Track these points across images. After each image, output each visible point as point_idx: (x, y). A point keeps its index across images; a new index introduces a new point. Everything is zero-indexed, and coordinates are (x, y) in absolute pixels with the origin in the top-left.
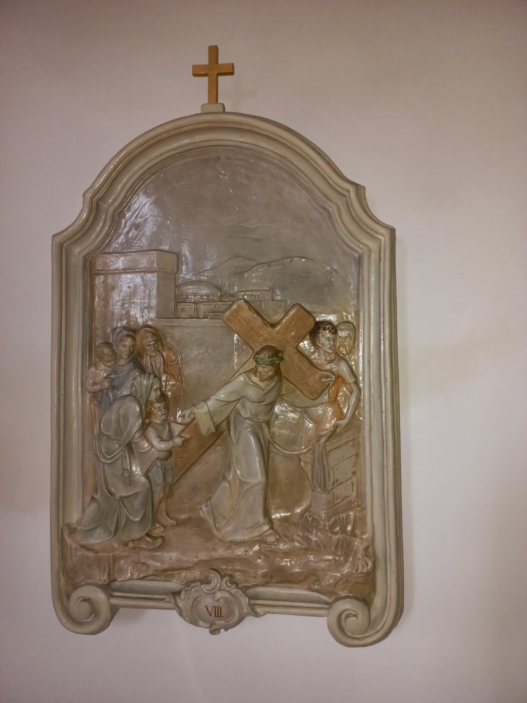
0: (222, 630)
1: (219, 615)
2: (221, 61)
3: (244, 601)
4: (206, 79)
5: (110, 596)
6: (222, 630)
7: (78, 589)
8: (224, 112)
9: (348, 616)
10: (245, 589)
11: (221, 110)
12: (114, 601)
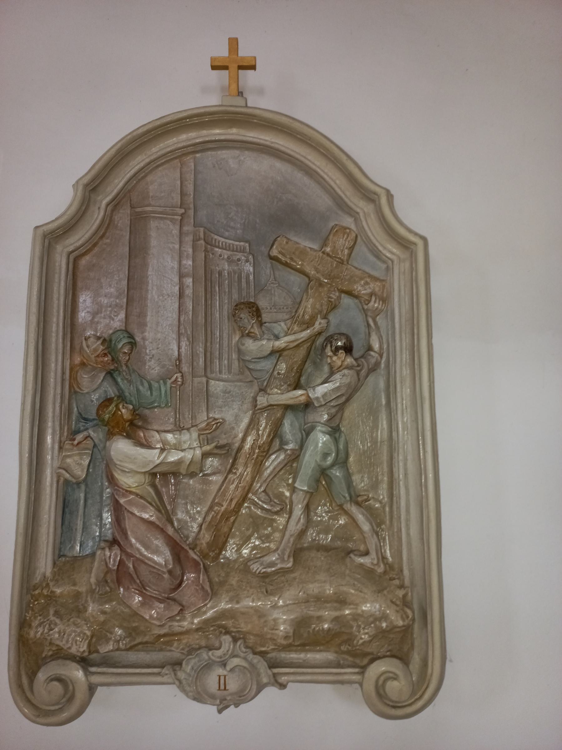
0: (232, 707)
2: (241, 54)
3: (262, 666)
4: (225, 73)
5: (87, 673)
6: (232, 707)
8: (246, 106)
10: (262, 654)
11: (245, 105)
12: (95, 679)
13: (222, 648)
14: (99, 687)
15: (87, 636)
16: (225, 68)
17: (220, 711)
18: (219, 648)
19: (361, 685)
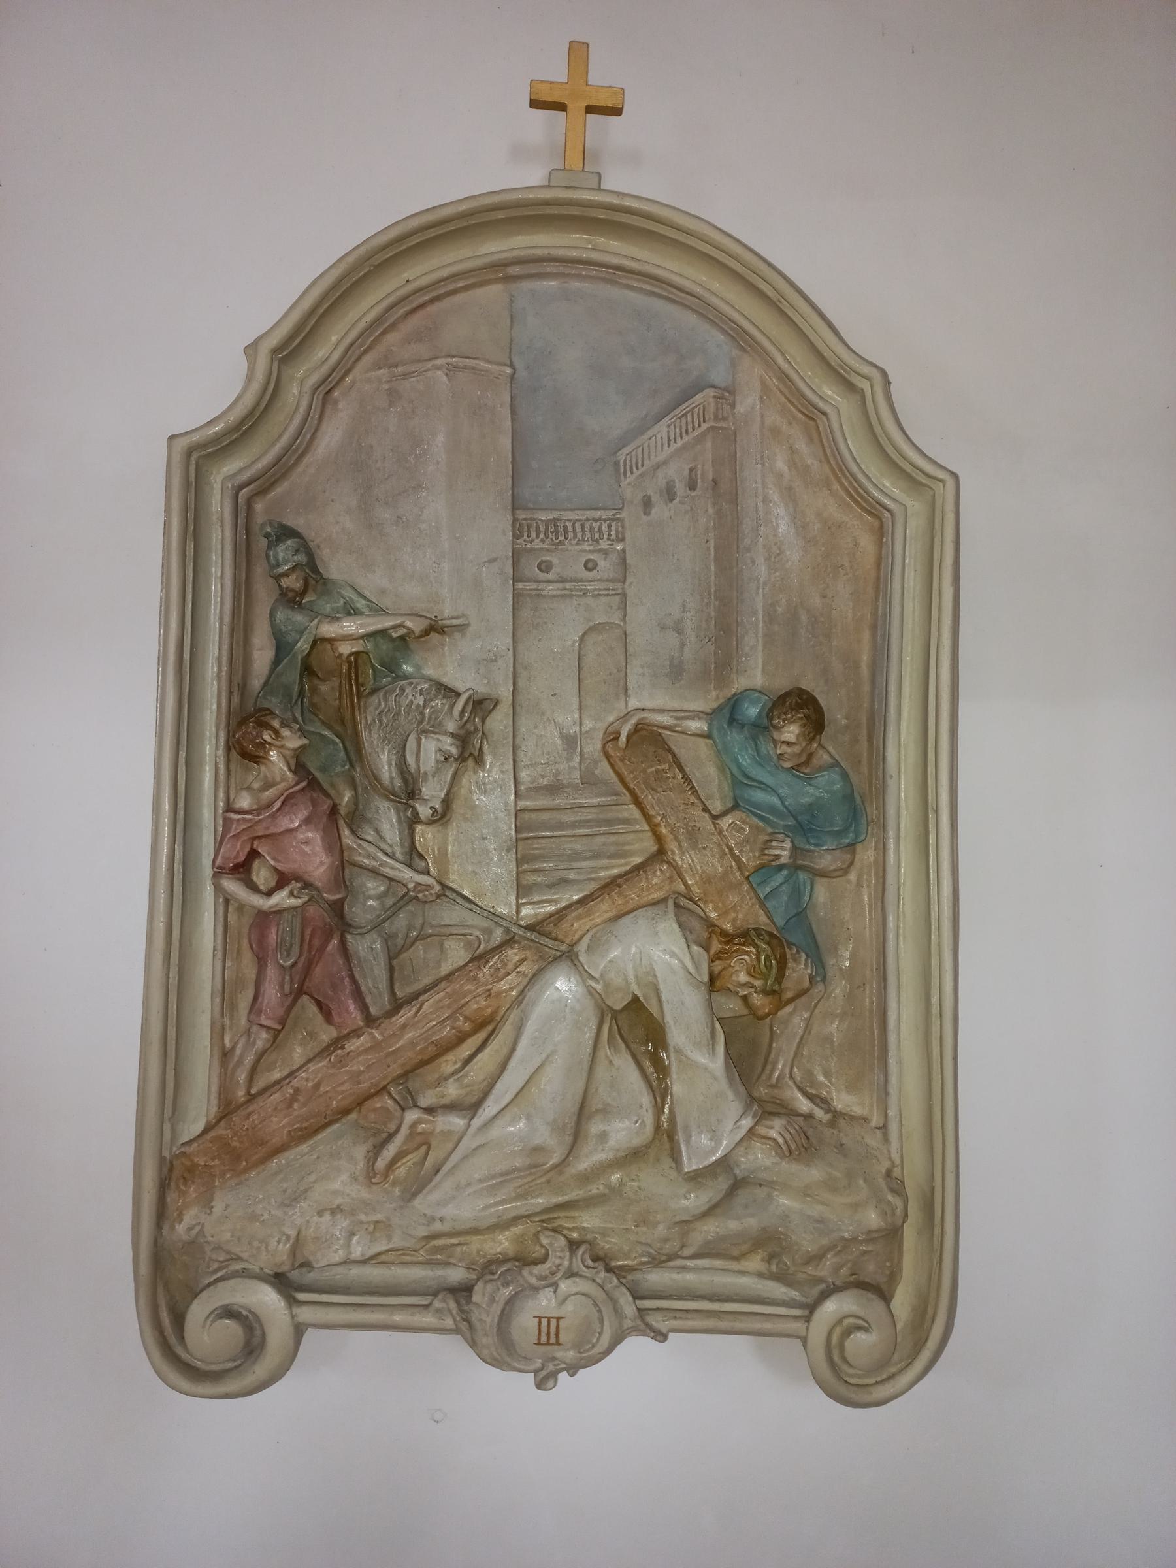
0: (563, 1376)
1: (553, 1340)
2: (594, 78)
5: (292, 1301)
6: (563, 1376)
7: (883, 1303)
8: (599, 189)
9: (847, 1333)
13: (549, 1261)
14: (309, 1329)
15: (288, 1237)
16: (561, 107)
17: (540, 1385)
18: (544, 1259)
19: (805, 1341)
